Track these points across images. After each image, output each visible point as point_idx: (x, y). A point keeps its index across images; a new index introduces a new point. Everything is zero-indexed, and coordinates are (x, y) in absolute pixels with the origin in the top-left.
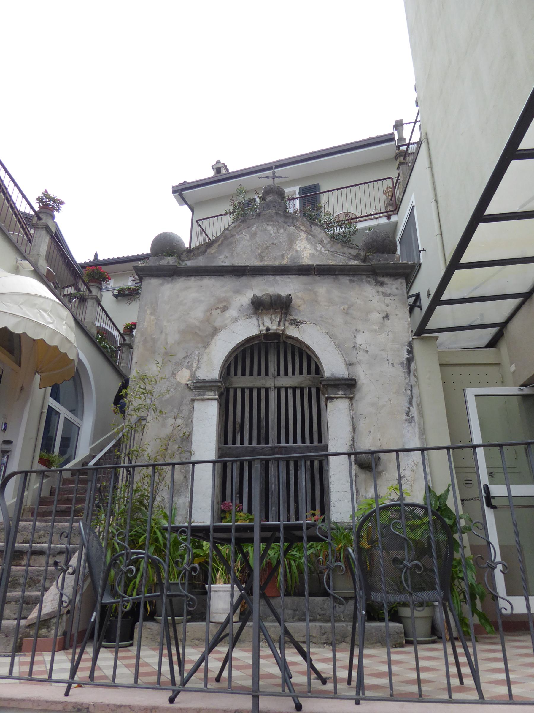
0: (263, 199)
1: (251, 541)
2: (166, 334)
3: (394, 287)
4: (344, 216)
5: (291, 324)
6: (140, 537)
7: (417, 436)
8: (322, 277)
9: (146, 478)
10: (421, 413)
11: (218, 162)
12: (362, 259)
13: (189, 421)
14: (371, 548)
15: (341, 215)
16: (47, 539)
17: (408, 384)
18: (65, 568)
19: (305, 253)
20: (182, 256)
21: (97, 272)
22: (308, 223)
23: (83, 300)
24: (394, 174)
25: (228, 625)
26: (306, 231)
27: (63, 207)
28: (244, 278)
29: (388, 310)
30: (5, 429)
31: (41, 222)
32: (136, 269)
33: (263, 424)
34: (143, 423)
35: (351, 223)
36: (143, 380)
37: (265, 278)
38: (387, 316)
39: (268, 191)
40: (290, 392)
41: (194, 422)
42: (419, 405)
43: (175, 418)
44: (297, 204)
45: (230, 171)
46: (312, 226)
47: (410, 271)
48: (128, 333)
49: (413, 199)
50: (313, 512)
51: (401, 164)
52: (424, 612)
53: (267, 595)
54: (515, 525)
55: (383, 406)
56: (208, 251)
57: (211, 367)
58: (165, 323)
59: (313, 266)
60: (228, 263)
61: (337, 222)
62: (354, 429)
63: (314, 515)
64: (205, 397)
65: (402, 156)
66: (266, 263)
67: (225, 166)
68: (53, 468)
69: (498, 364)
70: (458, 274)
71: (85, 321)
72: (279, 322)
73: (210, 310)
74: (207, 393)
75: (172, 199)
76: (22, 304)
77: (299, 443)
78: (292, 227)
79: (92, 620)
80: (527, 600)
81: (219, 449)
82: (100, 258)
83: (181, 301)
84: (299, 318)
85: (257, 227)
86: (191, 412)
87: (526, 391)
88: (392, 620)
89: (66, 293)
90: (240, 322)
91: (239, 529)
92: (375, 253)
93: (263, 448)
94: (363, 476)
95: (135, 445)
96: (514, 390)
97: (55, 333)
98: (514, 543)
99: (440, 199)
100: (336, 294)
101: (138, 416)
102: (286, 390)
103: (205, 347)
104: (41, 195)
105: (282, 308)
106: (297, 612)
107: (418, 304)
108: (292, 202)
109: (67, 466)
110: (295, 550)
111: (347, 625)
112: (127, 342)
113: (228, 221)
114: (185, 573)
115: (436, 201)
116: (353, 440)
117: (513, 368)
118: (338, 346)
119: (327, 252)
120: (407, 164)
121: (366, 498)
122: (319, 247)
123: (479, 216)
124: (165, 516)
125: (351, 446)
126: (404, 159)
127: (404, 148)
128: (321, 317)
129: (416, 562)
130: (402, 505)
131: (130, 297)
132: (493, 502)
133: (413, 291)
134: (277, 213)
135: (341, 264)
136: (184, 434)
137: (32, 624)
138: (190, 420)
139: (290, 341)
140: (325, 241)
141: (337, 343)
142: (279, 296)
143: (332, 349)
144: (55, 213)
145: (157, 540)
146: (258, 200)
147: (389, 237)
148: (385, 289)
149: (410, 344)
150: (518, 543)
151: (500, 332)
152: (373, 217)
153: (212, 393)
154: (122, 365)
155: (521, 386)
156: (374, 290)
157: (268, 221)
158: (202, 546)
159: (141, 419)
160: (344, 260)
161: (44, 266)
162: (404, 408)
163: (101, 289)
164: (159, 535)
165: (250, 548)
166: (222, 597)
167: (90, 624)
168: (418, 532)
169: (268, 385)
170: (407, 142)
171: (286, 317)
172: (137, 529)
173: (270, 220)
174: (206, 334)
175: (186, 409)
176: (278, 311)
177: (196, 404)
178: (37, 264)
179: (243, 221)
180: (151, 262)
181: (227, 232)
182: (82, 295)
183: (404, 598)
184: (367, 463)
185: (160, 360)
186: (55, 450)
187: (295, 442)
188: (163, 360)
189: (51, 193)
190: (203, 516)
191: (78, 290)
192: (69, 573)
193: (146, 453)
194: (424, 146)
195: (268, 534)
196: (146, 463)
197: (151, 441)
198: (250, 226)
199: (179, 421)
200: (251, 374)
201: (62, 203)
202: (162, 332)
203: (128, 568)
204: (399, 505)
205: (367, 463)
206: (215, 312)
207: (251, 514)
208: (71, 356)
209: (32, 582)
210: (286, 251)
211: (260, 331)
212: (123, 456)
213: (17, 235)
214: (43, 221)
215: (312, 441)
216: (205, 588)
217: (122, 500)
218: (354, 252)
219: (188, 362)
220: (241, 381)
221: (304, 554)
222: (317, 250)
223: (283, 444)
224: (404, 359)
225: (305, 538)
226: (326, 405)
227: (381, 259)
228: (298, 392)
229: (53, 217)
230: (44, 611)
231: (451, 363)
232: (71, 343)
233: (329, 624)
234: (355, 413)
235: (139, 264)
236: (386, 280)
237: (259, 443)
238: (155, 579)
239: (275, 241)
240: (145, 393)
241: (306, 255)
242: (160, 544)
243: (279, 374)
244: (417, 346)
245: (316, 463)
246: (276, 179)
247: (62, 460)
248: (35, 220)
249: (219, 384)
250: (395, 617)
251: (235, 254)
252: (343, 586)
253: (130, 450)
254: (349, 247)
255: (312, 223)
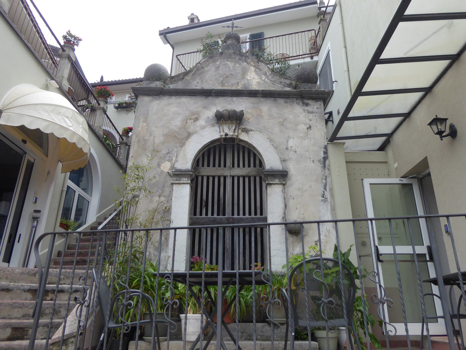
0: (224, 42)
1: (215, 283)
2: (154, 137)
3: (315, 107)
4: (281, 56)
5: (243, 131)
6: (134, 281)
7: (329, 211)
8: (265, 99)
9: (138, 239)
10: (332, 196)
11: (192, 14)
12: (293, 87)
13: (169, 198)
14: (296, 289)
15: (279, 55)
16: (69, 281)
17: (323, 175)
18: (82, 302)
19: (253, 81)
20: (167, 81)
21: (104, 90)
22: (256, 60)
23: (93, 110)
24: (316, 27)
25: (199, 342)
26: (254, 66)
27: (80, 43)
28: (210, 98)
29: (311, 123)
30: (35, 202)
31: (65, 53)
32: (134, 90)
33: (222, 201)
34: (137, 199)
35: (286, 61)
36: (137, 169)
37: (225, 98)
38: (310, 127)
39: (229, 37)
40: (241, 179)
41: (173, 199)
42: (331, 190)
43: (159, 196)
44: (248, 46)
45: (200, 21)
46: (259, 62)
47: (326, 96)
48: (125, 135)
49: (329, 45)
50: (256, 264)
51: (321, 20)
52: (332, 334)
53: (226, 322)
54: (399, 274)
55: (306, 190)
56: (185, 78)
57: (186, 161)
58: (153, 129)
59: (259, 91)
60: (199, 87)
61: (276, 60)
62: (286, 206)
63: (256, 266)
64: (181, 182)
65: (322, 15)
66: (226, 88)
67: (197, 17)
68: (70, 231)
69: (386, 162)
70: (360, 99)
71: (95, 125)
72: (235, 130)
73: (186, 120)
74: (182, 179)
75: (159, 40)
76: (50, 112)
77: (247, 216)
78: (245, 63)
79: (101, 339)
80: (406, 325)
81: (190, 219)
82: (105, 80)
83: (164, 114)
84: (249, 127)
85: (220, 62)
86: (171, 192)
87: (405, 181)
88: (313, 340)
89: (79, 105)
90: (207, 129)
91: (207, 275)
92: (303, 83)
93: (221, 218)
94: (291, 239)
95: (131, 215)
96: (397, 181)
97: (74, 133)
98: (398, 286)
99: (348, 47)
100: (275, 111)
101: (133, 195)
102: (238, 178)
103: (182, 146)
104: (65, 34)
105: (237, 120)
106: (244, 334)
107: (331, 119)
108: (244, 45)
109: (80, 230)
110: (244, 290)
111: (279, 343)
112: (125, 141)
113: (199, 57)
114: (168, 306)
115: (345, 47)
116: (285, 214)
117: (396, 165)
118: (276, 148)
119: (269, 81)
120: (326, 20)
121: (293, 254)
122: (264, 77)
123: (376, 60)
124: (152, 265)
125: (283, 218)
126: (324, 17)
127: (324, 9)
128: (264, 127)
129: (330, 299)
130: (321, 260)
131: (127, 109)
132: (381, 258)
133: (328, 110)
134: (234, 53)
135: (279, 90)
136: (166, 208)
137: (55, 343)
138: (170, 198)
139: (241, 143)
140: (268, 74)
141: (275, 145)
142: (235, 111)
143: (271, 149)
144: (75, 47)
145: (145, 283)
146: (220, 42)
147: (312, 72)
148: (309, 108)
149: (326, 148)
150: (401, 286)
151: (387, 141)
152: (300, 57)
153: (186, 179)
154: (120, 157)
155: (402, 177)
156: (301, 109)
157: (228, 58)
158: (178, 287)
159: (134, 197)
160: (281, 87)
161: (66, 85)
162: (320, 192)
163: (107, 103)
164: (148, 279)
165: (211, 289)
166: (193, 323)
167: (100, 342)
168: (329, 278)
169: (225, 174)
170: (326, 5)
171: (239, 126)
172: (132, 274)
173: (229, 57)
174: (181, 138)
175: (167, 190)
176: (234, 122)
177: (175, 186)
178: (61, 84)
179: (210, 58)
180: (144, 85)
181: (199, 65)
182: (92, 107)
183: (321, 323)
184: (295, 230)
185: (149, 155)
186: (71, 218)
187: (244, 214)
188: (152, 155)
189: (73, 33)
190: (181, 267)
191: (89, 102)
192: (85, 305)
193: (138, 221)
194: (338, 9)
195: (228, 279)
196: (138, 228)
197: (142, 212)
198: (215, 61)
199: (162, 199)
200: (214, 166)
201: (80, 40)
202: (151, 135)
203: (128, 302)
204: (319, 260)
205: (295, 230)
206: (189, 122)
207: (212, 265)
208: (85, 150)
209: (55, 312)
210: (240, 80)
211: (221, 136)
212: (122, 222)
213: (47, 61)
214: (67, 52)
215: (256, 214)
216: (179, 317)
217: (120, 254)
218: (288, 82)
219: (169, 157)
220: (206, 171)
221: (250, 295)
222: (262, 80)
223: (236, 216)
224: (321, 158)
225: (254, 282)
226: (266, 189)
227: (307, 88)
228: (247, 180)
229: (74, 50)
230: (67, 332)
231: (354, 161)
232: (85, 140)
233: (269, 342)
234: (287, 195)
235: (134, 85)
236: (310, 102)
237: (218, 215)
238: (144, 310)
239: (233, 73)
240: (138, 178)
241: (254, 83)
242: (148, 286)
243: (233, 166)
244: (331, 149)
245: (259, 230)
246: (234, 28)
247: (76, 224)
248: (61, 51)
249: (191, 173)
250: (314, 338)
251: (204, 81)
252: (276, 315)
253: (127, 219)
254: (285, 78)
255: (259, 60)
